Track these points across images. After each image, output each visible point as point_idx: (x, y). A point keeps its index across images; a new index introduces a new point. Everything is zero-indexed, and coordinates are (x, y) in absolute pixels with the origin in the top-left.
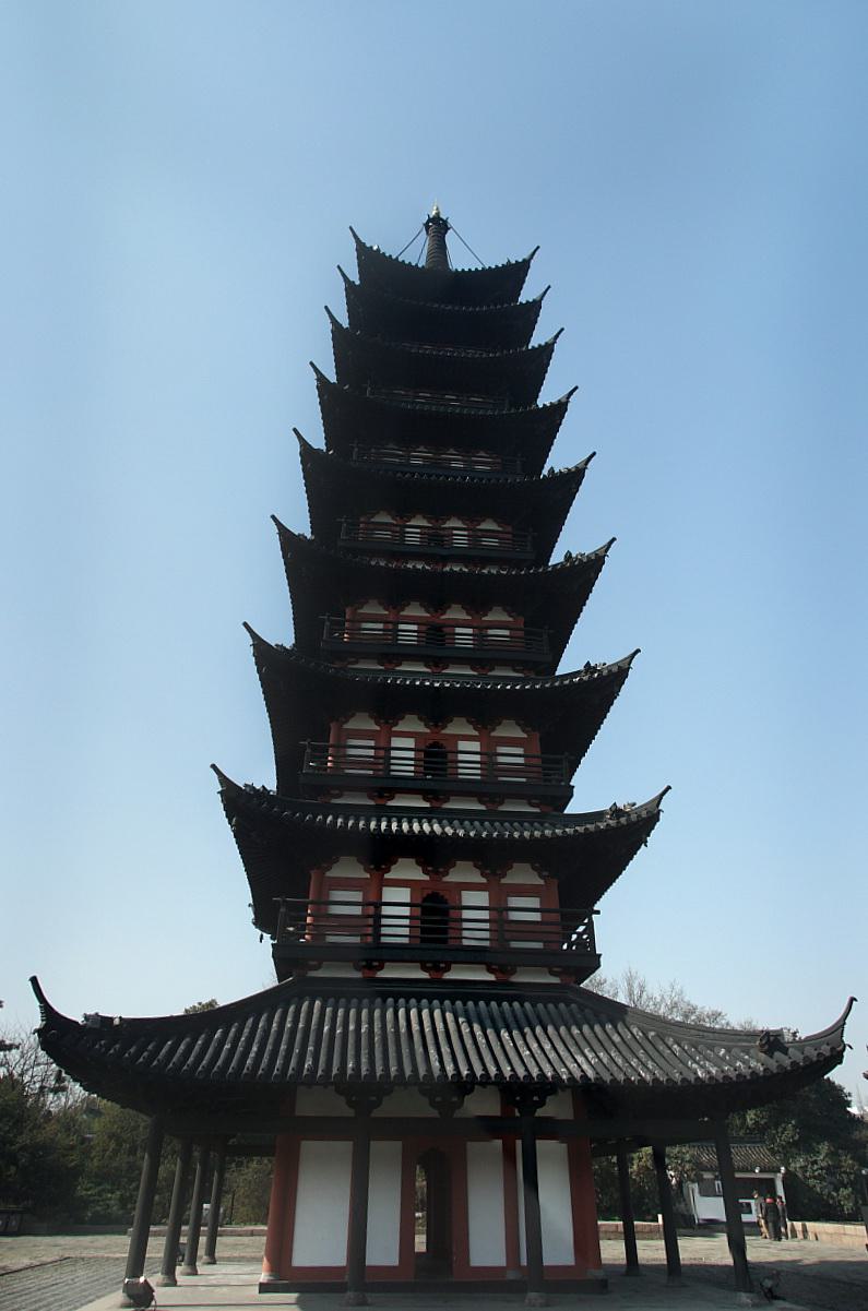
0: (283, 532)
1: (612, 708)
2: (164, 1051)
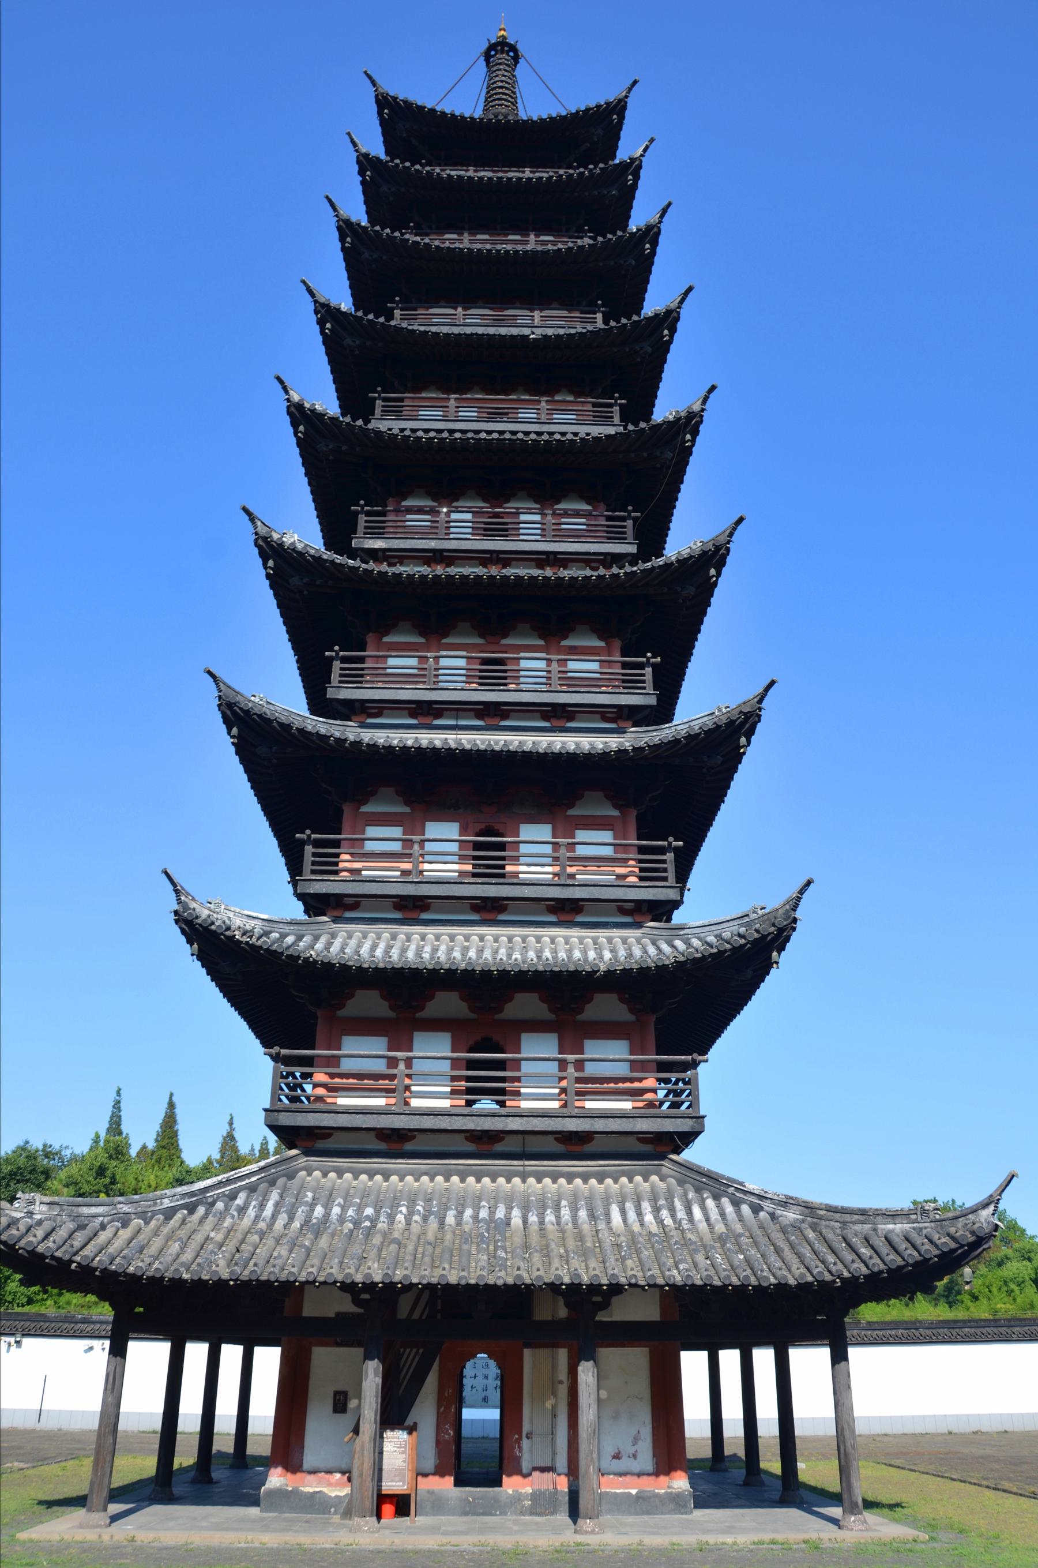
0: (270, 550)
1: (666, 366)
2: (465, 242)
